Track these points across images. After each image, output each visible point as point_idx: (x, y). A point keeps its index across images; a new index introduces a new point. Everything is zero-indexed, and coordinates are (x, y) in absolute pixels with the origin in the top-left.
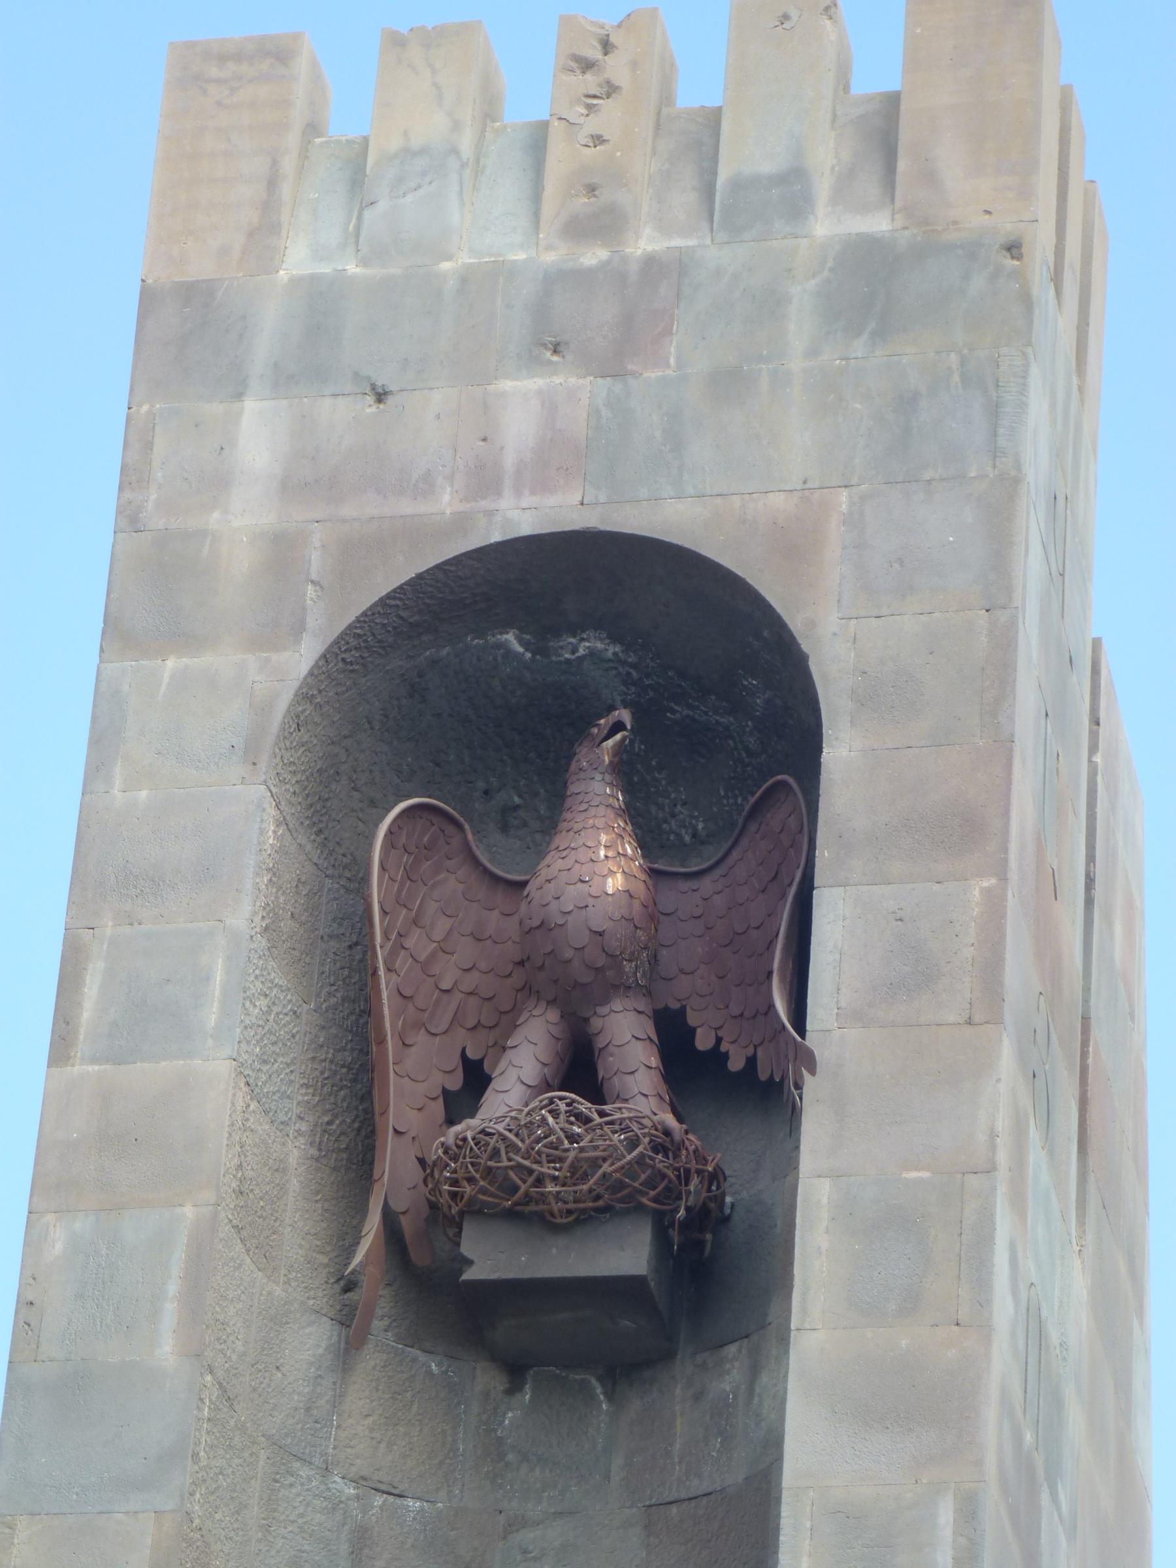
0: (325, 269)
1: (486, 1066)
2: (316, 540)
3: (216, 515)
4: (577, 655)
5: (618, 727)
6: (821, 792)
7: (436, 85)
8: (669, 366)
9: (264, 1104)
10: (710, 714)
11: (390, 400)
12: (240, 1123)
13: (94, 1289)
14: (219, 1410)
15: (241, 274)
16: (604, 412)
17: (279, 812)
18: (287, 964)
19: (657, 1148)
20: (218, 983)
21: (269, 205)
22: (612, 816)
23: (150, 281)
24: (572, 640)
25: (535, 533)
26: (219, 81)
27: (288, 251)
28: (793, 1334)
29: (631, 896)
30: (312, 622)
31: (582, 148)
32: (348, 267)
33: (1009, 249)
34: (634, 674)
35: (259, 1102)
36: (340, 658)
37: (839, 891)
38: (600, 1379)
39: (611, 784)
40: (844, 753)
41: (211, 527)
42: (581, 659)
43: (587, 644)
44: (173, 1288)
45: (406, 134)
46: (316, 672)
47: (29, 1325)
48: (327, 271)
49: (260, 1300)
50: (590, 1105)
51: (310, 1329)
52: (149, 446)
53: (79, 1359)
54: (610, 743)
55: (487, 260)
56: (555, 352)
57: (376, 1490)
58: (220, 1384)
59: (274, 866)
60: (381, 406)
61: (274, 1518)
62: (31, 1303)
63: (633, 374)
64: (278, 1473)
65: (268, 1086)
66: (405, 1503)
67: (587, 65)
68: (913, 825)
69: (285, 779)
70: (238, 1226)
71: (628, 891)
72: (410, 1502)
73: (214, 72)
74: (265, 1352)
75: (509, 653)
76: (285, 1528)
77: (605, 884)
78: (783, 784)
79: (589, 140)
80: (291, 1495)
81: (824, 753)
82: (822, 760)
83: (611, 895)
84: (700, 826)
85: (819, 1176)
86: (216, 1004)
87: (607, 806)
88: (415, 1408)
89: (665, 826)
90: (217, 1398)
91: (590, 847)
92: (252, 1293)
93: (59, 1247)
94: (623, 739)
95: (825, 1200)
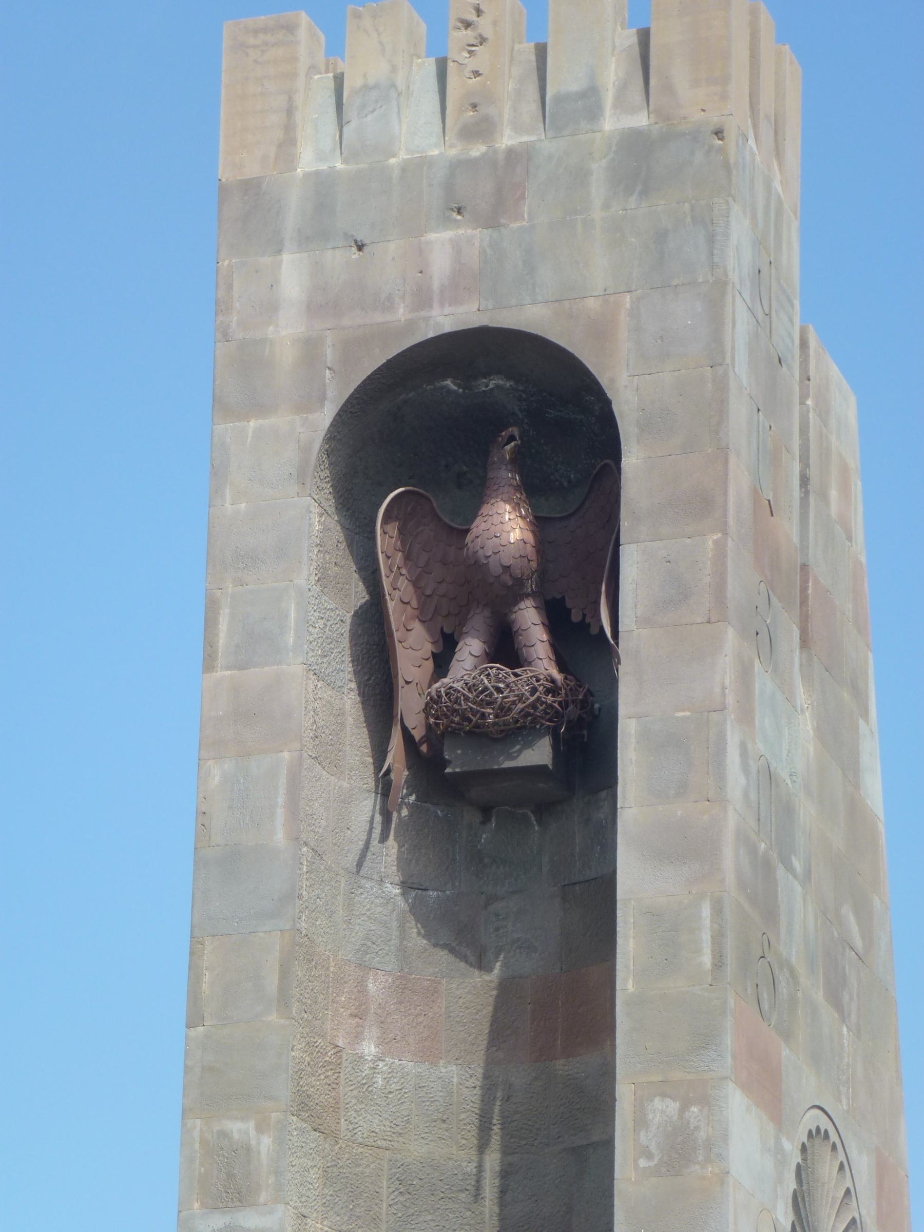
0: (323, 167)
1: (456, 637)
2: (329, 342)
3: (271, 328)
4: (489, 388)
5: (512, 438)
6: (622, 486)
7: (381, 43)
8: (524, 219)
9: (327, 681)
10: (571, 414)
11: (366, 249)
12: (312, 698)
13: (238, 803)
14: (314, 863)
15: (275, 173)
16: (488, 251)
17: (321, 508)
18: (335, 594)
19: (548, 691)
20: (292, 618)
21: (289, 128)
22: (513, 491)
23: (224, 180)
24: (484, 380)
25: (453, 331)
26: (255, 47)
27: (302, 155)
28: (619, 810)
29: (525, 543)
30: (330, 393)
31: (467, 79)
32: (336, 165)
33: (716, 134)
34: (524, 396)
35: (323, 681)
36: (348, 412)
37: (633, 547)
38: (532, 812)
39: (511, 471)
40: (634, 461)
41: (269, 336)
42: (492, 390)
43: (494, 382)
44: (281, 800)
45: (365, 76)
46: (334, 423)
47: (204, 826)
48: (325, 168)
49: (334, 793)
50: (508, 670)
51: (366, 802)
52: (230, 287)
53: (233, 844)
54: (508, 447)
55: (416, 156)
56: (459, 213)
57: (410, 888)
58: (313, 849)
59: (320, 542)
60: (361, 253)
61: (352, 915)
62: (204, 813)
63: (504, 226)
64: (353, 889)
65: (328, 669)
66: (428, 893)
67: (468, 25)
68: (674, 503)
69: (323, 488)
70: (316, 757)
71: (523, 539)
72: (431, 893)
73: (251, 41)
74: (340, 821)
75: (449, 391)
76: (360, 919)
77: (509, 536)
78: (606, 464)
79: (472, 74)
80: (362, 900)
81: (622, 462)
82: (622, 465)
83: (513, 543)
84: (572, 476)
85: (630, 718)
86: (292, 632)
87: (509, 485)
88: (430, 838)
89: (552, 477)
90: (312, 858)
91: (500, 514)
92: (329, 790)
93: (217, 779)
94: (516, 446)
95: (633, 731)
